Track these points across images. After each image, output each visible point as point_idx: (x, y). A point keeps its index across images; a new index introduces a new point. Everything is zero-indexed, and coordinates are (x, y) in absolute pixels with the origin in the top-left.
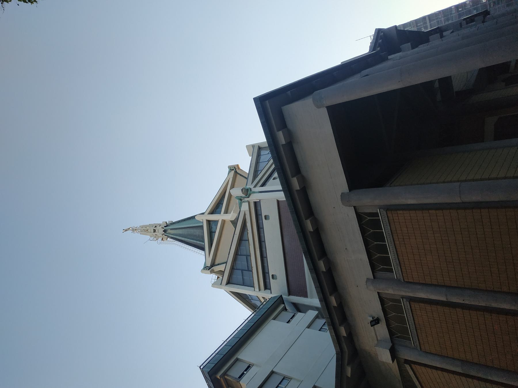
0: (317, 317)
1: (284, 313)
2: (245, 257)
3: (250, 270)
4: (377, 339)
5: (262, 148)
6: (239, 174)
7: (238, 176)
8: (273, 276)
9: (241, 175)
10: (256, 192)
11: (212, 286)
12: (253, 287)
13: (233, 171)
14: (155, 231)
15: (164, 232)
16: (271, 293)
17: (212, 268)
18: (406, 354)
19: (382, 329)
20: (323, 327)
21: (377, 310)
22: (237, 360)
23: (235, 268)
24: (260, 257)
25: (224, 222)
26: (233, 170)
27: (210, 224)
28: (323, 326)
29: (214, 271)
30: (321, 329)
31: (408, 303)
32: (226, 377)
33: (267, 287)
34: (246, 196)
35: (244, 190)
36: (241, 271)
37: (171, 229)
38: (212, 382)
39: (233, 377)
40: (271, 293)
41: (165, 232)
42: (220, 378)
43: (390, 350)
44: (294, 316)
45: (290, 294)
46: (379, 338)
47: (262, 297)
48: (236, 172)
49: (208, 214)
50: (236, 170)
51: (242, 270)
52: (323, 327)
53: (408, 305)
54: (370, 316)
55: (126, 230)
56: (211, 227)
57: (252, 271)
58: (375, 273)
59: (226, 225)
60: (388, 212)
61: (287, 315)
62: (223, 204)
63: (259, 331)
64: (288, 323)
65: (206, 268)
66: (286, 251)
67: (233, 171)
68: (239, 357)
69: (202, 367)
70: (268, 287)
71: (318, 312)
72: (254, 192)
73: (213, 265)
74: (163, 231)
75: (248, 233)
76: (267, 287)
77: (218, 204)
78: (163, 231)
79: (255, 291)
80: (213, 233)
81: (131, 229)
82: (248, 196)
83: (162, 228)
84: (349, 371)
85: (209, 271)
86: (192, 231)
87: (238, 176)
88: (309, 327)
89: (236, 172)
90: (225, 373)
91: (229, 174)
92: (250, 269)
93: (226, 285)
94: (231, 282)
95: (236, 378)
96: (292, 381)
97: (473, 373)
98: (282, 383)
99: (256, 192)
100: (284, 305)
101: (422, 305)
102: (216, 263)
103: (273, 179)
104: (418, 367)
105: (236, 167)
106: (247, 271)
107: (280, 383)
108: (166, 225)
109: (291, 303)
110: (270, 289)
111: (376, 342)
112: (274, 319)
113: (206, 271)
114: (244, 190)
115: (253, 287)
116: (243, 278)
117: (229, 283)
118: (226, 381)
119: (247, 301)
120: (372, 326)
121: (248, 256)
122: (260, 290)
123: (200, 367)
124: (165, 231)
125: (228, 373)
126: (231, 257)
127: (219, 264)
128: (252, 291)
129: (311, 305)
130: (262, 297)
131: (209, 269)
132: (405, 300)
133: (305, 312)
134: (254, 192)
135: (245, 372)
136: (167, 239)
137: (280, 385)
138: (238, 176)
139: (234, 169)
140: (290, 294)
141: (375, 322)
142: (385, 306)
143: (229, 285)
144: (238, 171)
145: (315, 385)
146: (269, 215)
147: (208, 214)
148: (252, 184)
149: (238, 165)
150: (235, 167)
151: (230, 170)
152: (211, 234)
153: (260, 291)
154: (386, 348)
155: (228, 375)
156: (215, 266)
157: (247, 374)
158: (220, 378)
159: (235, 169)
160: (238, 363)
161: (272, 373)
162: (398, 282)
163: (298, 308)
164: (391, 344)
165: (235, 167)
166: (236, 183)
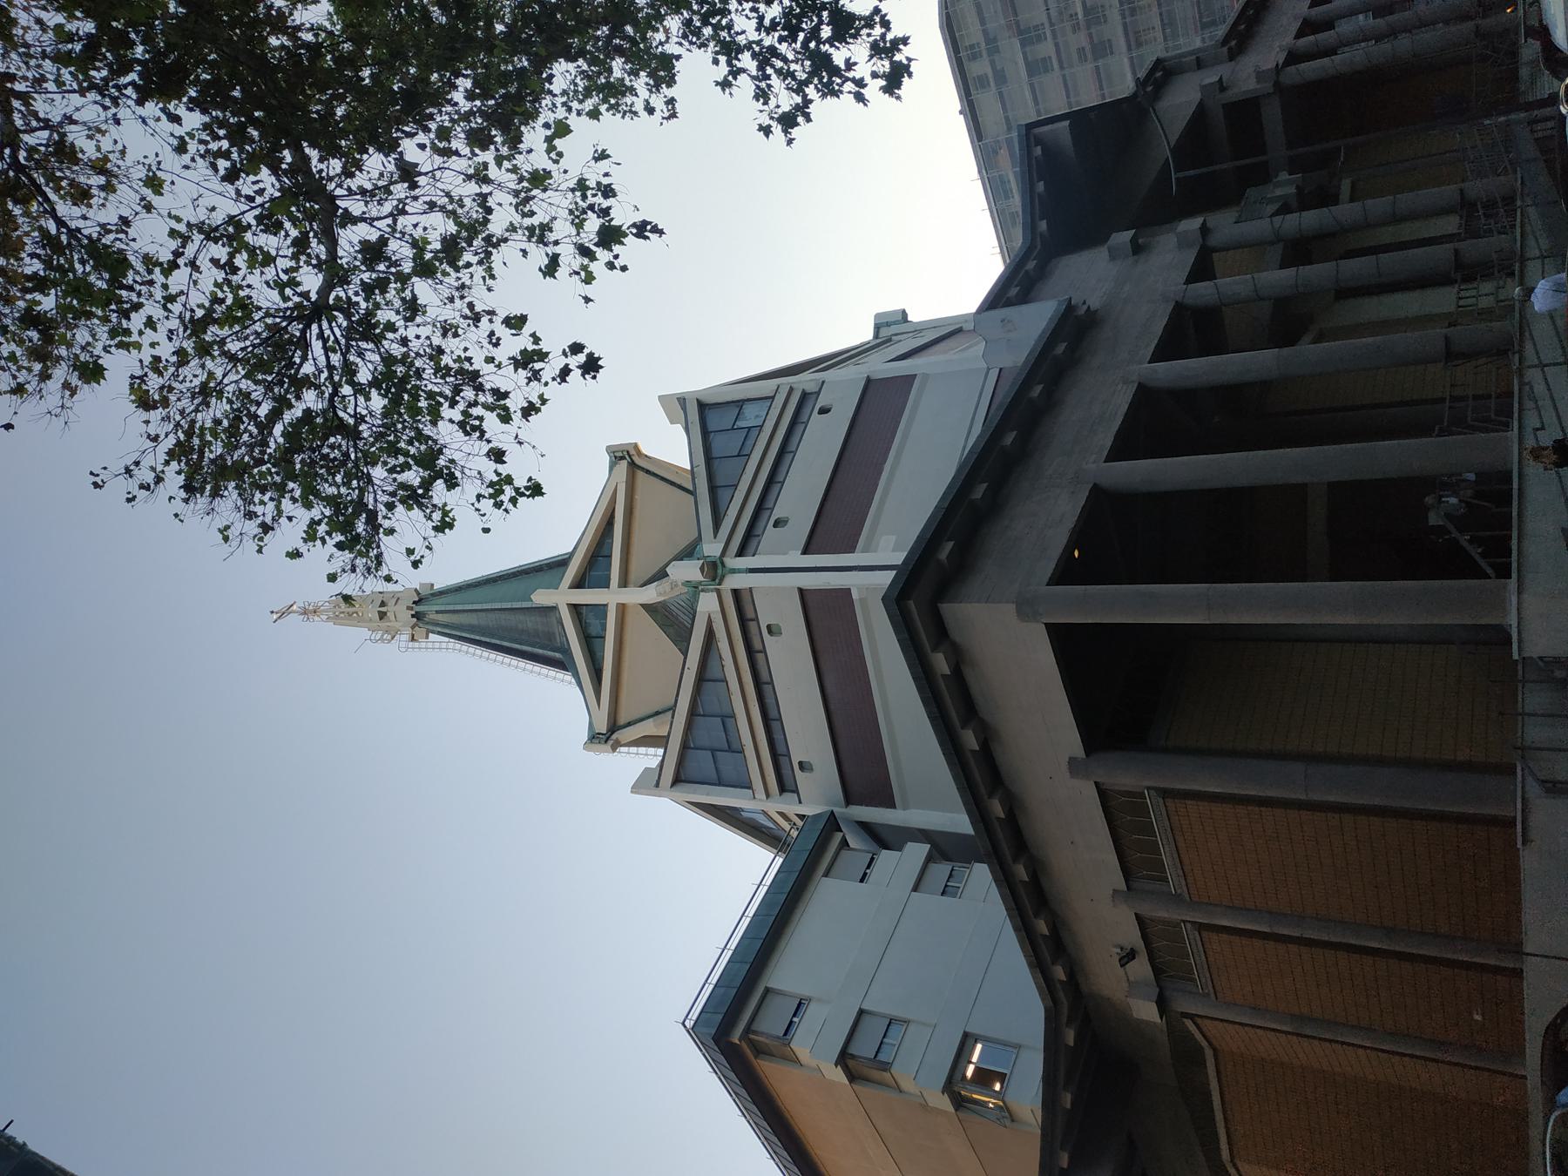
0: (929, 859)
1: (844, 853)
2: (719, 719)
3: (735, 749)
4: (1128, 980)
5: (707, 405)
6: (643, 469)
7: (640, 475)
8: (800, 763)
9: (648, 472)
10: (739, 571)
11: (632, 792)
12: (750, 787)
13: (624, 464)
14: (382, 615)
15: (415, 620)
16: (800, 802)
17: (614, 736)
18: (1183, 1004)
19: (1141, 968)
20: (949, 884)
21: (1134, 937)
22: (767, 991)
23: (692, 746)
24: (622, 544)
25: (622, 609)
26: (622, 458)
27: (581, 614)
28: (948, 881)
29: (620, 742)
30: (947, 889)
31: (1197, 933)
32: (752, 1036)
33: (785, 786)
34: (714, 580)
35: (706, 569)
36: (709, 753)
37: (437, 612)
38: (723, 1054)
39: (768, 1036)
40: (800, 802)
41: (418, 619)
42: (738, 1043)
43: (1156, 1003)
44: (872, 859)
45: (849, 800)
46: (1132, 979)
47: (777, 812)
48: (632, 464)
49: (569, 588)
50: (634, 458)
51: (713, 751)
52: (949, 884)
53: (1198, 938)
54: (1116, 946)
55: (282, 615)
56: (586, 623)
57: (742, 751)
58: (1131, 882)
59: (629, 619)
60: (1166, 800)
61: (854, 859)
62: (610, 556)
63: (798, 912)
64: (862, 881)
65: (595, 738)
66: (832, 707)
67: (624, 464)
68: (771, 985)
69: (689, 1024)
70: (788, 783)
71: (929, 846)
72: (733, 571)
73: (614, 727)
74: (413, 616)
75: (723, 666)
76: (785, 786)
77: (592, 556)
78: (413, 616)
79: (754, 798)
80: (593, 640)
81: (295, 607)
82: (717, 581)
83: (409, 608)
84: (1070, 1037)
85: (608, 747)
86: (512, 620)
87: (640, 474)
88: (915, 889)
89: (632, 464)
90: (748, 1029)
91: (614, 471)
92: (735, 746)
93: (672, 786)
94: (683, 778)
95: (778, 1038)
96: (912, 1028)
97: (1308, 1032)
98: (888, 1034)
99: (739, 571)
100: (841, 834)
101: (1225, 937)
102: (622, 721)
103: (775, 526)
104: (1207, 1022)
105: (633, 452)
106: (726, 751)
107: (884, 1037)
108: (417, 599)
109: (858, 822)
110: (796, 791)
111: (1125, 985)
112: (826, 874)
113: (602, 746)
114: (706, 569)
115: (750, 787)
116: (716, 768)
117: (677, 781)
118: (752, 1044)
119: (727, 813)
120: (1122, 966)
121: (727, 718)
122: (768, 795)
123: (683, 1024)
124: (417, 616)
125: (754, 1027)
126: (681, 723)
127: (629, 724)
128: (749, 800)
129: (907, 825)
130: (777, 812)
131: (606, 742)
132: (1189, 925)
133: (900, 849)
134: (734, 569)
135: (795, 1019)
136: (427, 637)
137: (885, 1040)
138: (640, 475)
139: (627, 457)
140: (849, 800)
141: (1129, 956)
142: (1154, 945)
143: (680, 786)
144: (636, 459)
145: (967, 1030)
146: (781, 625)
147: (569, 588)
148: (715, 537)
149: (636, 446)
150: (628, 452)
151: (613, 458)
152: (591, 644)
153: (769, 800)
154: (1150, 1000)
155: (755, 1033)
156: (618, 730)
157: (803, 1020)
158: (738, 1043)
159: (630, 456)
160: (769, 997)
161: (861, 1012)
162: (1177, 899)
163: (883, 838)
164: (1158, 990)
165: (628, 452)
166: (636, 497)
